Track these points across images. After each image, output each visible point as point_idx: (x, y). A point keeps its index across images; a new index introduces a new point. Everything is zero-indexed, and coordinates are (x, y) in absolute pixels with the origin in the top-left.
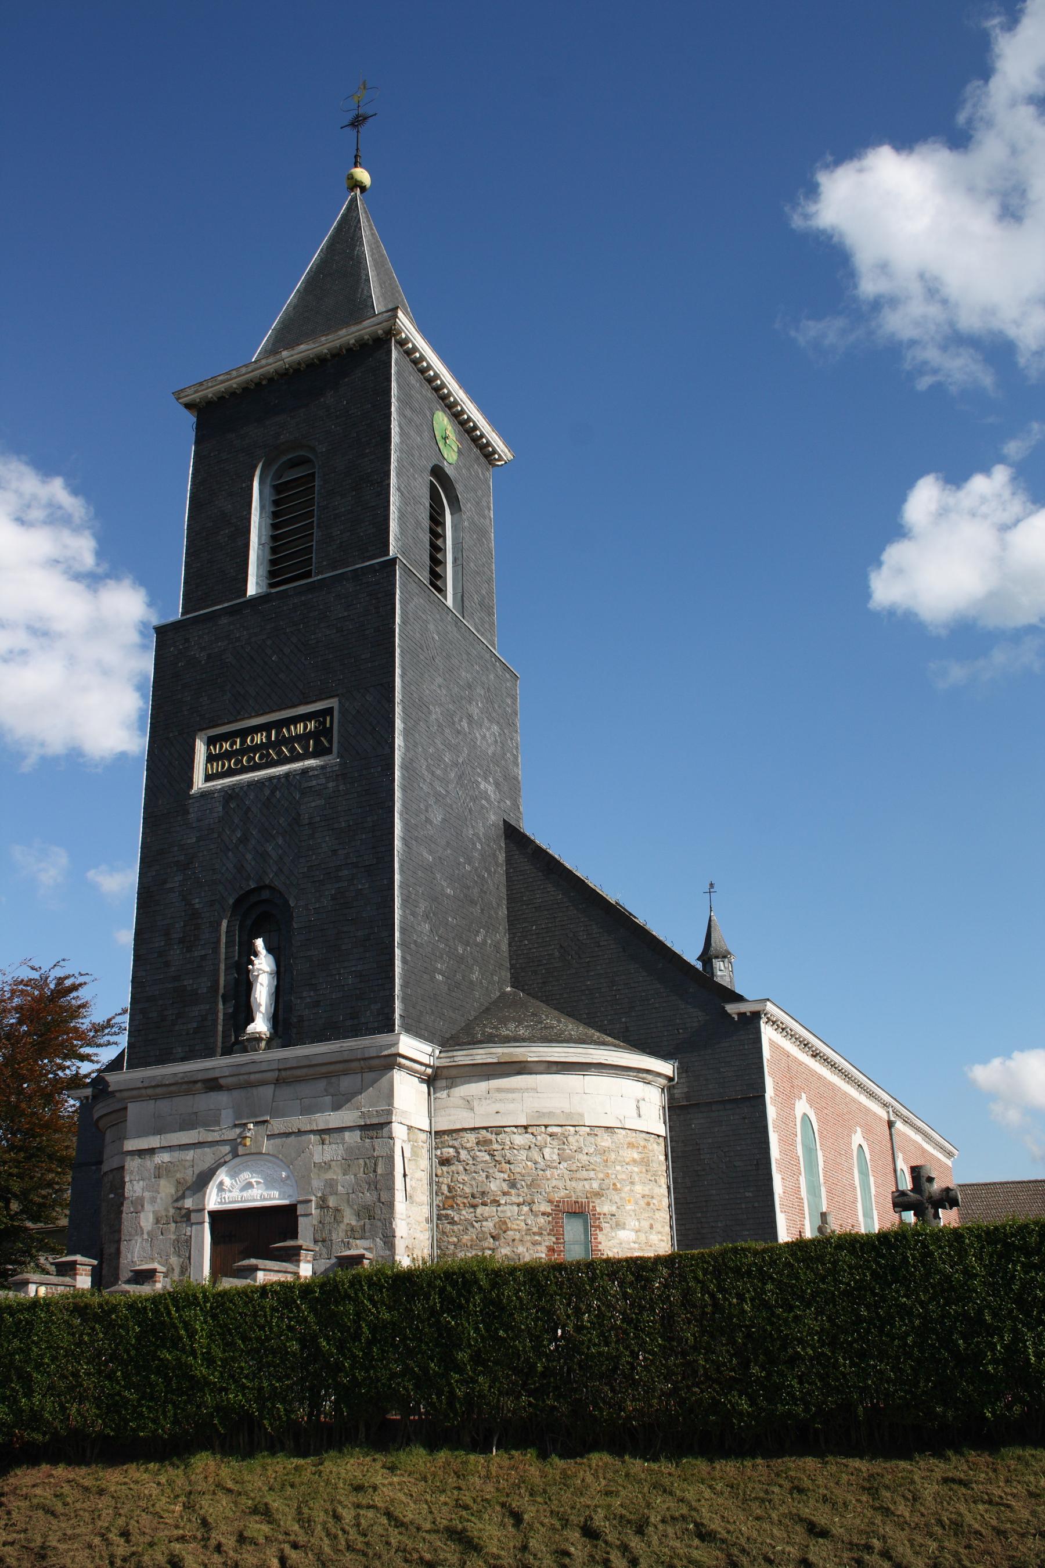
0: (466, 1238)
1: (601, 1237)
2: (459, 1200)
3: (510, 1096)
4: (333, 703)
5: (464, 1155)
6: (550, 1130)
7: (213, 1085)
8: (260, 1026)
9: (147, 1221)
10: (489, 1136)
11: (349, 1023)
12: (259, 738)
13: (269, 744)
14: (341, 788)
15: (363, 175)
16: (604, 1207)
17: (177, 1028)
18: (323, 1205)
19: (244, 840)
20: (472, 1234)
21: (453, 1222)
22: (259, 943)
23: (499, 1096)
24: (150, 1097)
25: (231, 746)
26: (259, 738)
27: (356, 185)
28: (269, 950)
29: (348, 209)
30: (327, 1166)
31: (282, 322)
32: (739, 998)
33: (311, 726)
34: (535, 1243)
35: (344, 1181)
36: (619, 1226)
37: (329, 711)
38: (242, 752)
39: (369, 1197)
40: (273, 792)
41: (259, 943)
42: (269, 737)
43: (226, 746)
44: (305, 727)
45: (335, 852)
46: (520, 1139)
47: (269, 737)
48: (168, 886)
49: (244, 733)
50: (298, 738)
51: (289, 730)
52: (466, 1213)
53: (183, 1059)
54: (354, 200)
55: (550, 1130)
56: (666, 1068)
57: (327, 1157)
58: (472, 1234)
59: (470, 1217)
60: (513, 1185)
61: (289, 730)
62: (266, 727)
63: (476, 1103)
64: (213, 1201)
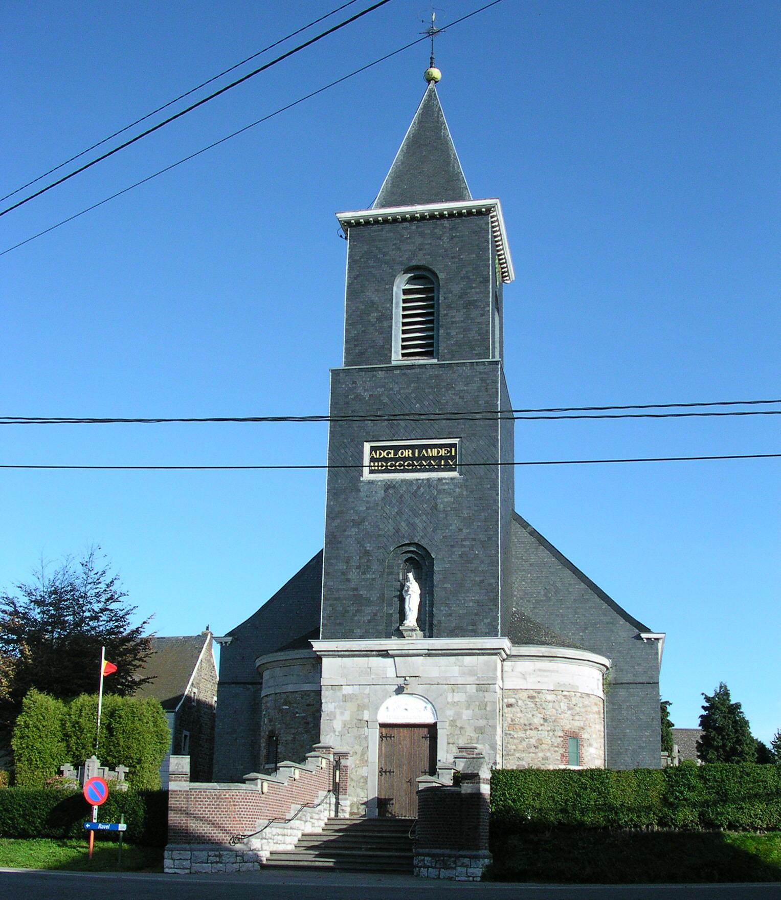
0: (520, 747)
1: (583, 751)
2: (517, 727)
3: (545, 674)
4: (456, 441)
5: (520, 703)
6: (564, 693)
7: (384, 654)
8: (411, 619)
9: (338, 725)
10: (534, 694)
11: (471, 628)
12: (407, 453)
13: (413, 458)
14: (465, 493)
15: (436, 73)
16: (585, 736)
17: (356, 618)
18: (453, 724)
19: (400, 513)
20: (524, 744)
21: (513, 738)
22: (411, 575)
23: (539, 673)
24: (339, 656)
25: (388, 454)
26: (407, 453)
27: (430, 79)
28: (416, 579)
29: (429, 96)
30: (456, 704)
31: (394, 172)
32: (648, 630)
33: (443, 452)
34: (555, 751)
35: (467, 714)
36: (590, 745)
37: (454, 445)
38: (396, 460)
39: (482, 723)
40: (419, 488)
41: (411, 575)
42: (413, 453)
43: (384, 454)
44: (438, 452)
45: (461, 530)
46: (550, 697)
47: (413, 453)
48: (346, 533)
49: (396, 448)
50: (433, 458)
51: (427, 452)
52: (521, 734)
53: (362, 637)
54: (432, 91)
55: (564, 693)
56: (607, 662)
57: (456, 700)
58: (524, 744)
59: (523, 735)
60: (545, 720)
61: (427, 452)
62: (412, 447)
63: (527, 676)
64: (386, 716)
